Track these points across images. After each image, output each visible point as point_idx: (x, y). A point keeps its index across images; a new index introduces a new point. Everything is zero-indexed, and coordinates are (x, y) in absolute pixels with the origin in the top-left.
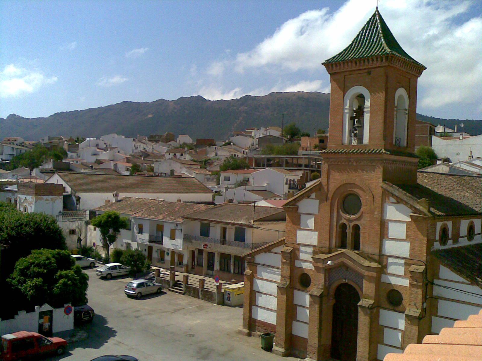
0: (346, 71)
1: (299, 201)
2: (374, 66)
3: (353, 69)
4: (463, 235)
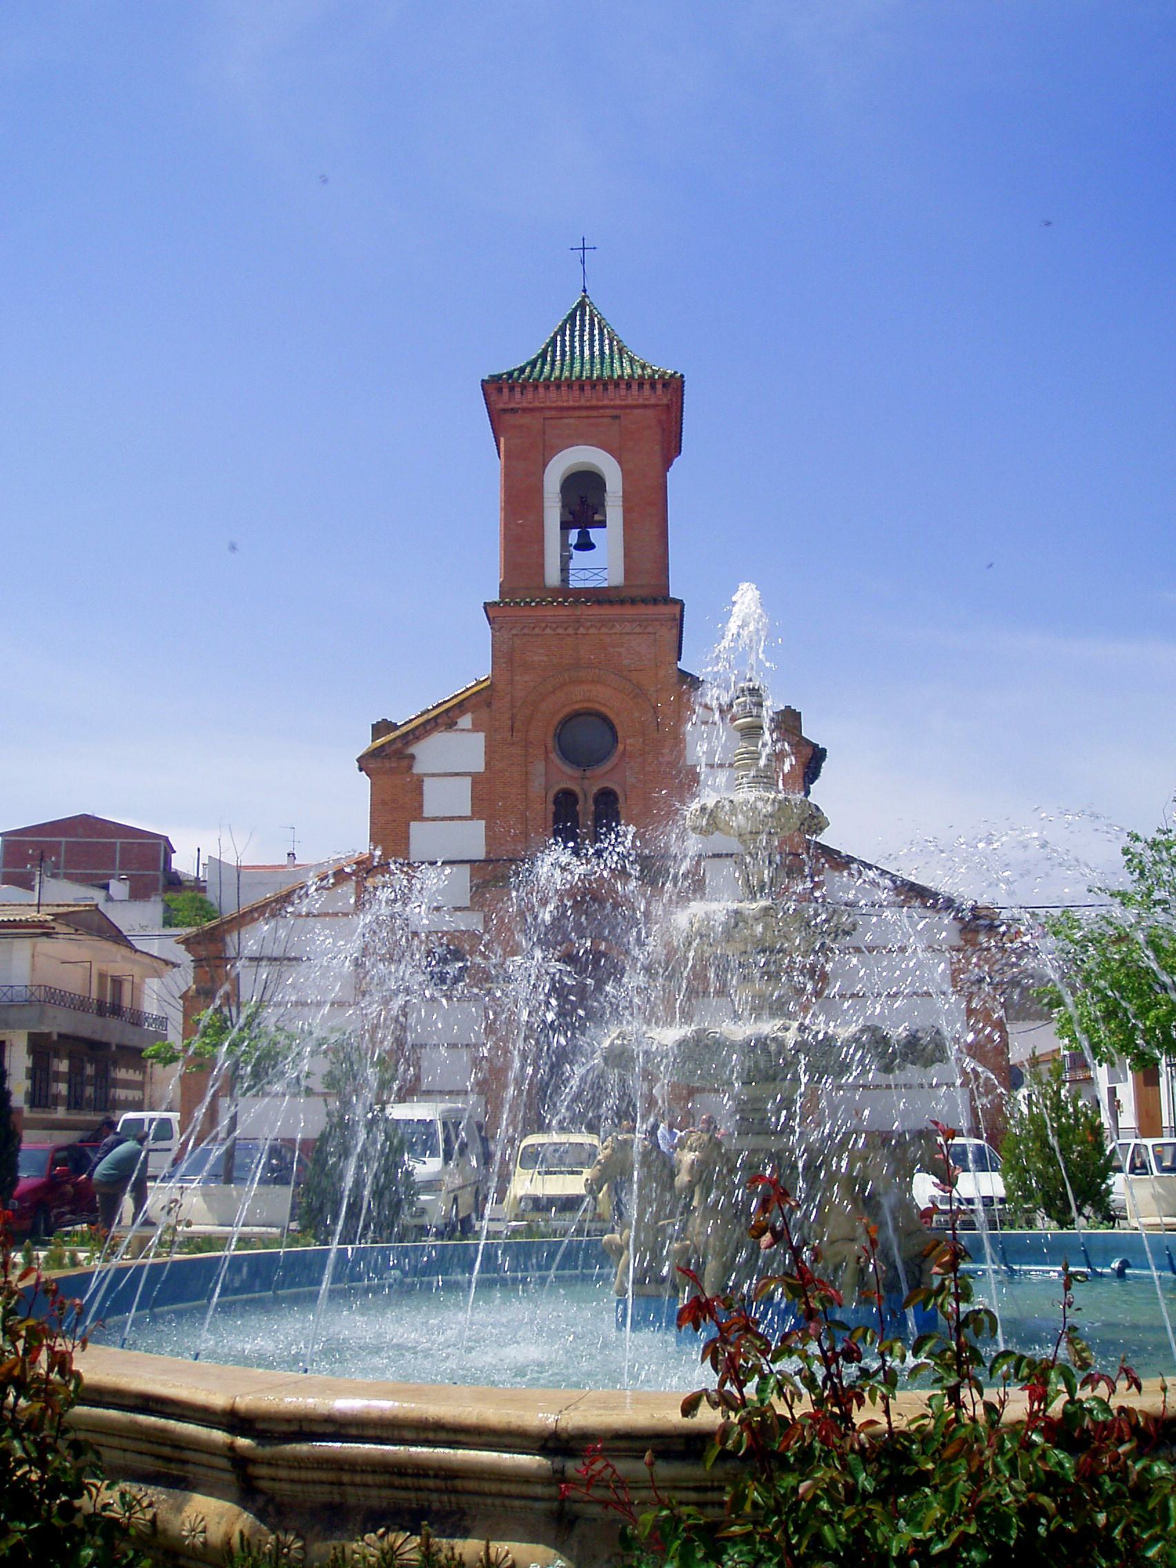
0: (550, 408)
1: (418, 739)
2: (630, 402)
3: (571, 404)
4: (430, 816)
